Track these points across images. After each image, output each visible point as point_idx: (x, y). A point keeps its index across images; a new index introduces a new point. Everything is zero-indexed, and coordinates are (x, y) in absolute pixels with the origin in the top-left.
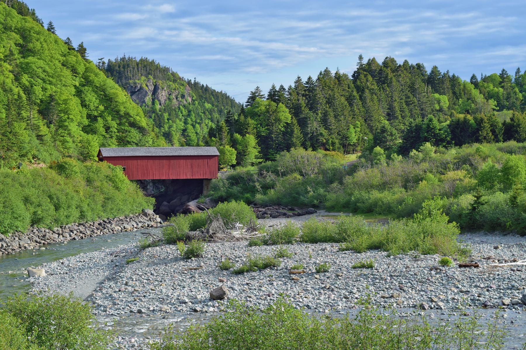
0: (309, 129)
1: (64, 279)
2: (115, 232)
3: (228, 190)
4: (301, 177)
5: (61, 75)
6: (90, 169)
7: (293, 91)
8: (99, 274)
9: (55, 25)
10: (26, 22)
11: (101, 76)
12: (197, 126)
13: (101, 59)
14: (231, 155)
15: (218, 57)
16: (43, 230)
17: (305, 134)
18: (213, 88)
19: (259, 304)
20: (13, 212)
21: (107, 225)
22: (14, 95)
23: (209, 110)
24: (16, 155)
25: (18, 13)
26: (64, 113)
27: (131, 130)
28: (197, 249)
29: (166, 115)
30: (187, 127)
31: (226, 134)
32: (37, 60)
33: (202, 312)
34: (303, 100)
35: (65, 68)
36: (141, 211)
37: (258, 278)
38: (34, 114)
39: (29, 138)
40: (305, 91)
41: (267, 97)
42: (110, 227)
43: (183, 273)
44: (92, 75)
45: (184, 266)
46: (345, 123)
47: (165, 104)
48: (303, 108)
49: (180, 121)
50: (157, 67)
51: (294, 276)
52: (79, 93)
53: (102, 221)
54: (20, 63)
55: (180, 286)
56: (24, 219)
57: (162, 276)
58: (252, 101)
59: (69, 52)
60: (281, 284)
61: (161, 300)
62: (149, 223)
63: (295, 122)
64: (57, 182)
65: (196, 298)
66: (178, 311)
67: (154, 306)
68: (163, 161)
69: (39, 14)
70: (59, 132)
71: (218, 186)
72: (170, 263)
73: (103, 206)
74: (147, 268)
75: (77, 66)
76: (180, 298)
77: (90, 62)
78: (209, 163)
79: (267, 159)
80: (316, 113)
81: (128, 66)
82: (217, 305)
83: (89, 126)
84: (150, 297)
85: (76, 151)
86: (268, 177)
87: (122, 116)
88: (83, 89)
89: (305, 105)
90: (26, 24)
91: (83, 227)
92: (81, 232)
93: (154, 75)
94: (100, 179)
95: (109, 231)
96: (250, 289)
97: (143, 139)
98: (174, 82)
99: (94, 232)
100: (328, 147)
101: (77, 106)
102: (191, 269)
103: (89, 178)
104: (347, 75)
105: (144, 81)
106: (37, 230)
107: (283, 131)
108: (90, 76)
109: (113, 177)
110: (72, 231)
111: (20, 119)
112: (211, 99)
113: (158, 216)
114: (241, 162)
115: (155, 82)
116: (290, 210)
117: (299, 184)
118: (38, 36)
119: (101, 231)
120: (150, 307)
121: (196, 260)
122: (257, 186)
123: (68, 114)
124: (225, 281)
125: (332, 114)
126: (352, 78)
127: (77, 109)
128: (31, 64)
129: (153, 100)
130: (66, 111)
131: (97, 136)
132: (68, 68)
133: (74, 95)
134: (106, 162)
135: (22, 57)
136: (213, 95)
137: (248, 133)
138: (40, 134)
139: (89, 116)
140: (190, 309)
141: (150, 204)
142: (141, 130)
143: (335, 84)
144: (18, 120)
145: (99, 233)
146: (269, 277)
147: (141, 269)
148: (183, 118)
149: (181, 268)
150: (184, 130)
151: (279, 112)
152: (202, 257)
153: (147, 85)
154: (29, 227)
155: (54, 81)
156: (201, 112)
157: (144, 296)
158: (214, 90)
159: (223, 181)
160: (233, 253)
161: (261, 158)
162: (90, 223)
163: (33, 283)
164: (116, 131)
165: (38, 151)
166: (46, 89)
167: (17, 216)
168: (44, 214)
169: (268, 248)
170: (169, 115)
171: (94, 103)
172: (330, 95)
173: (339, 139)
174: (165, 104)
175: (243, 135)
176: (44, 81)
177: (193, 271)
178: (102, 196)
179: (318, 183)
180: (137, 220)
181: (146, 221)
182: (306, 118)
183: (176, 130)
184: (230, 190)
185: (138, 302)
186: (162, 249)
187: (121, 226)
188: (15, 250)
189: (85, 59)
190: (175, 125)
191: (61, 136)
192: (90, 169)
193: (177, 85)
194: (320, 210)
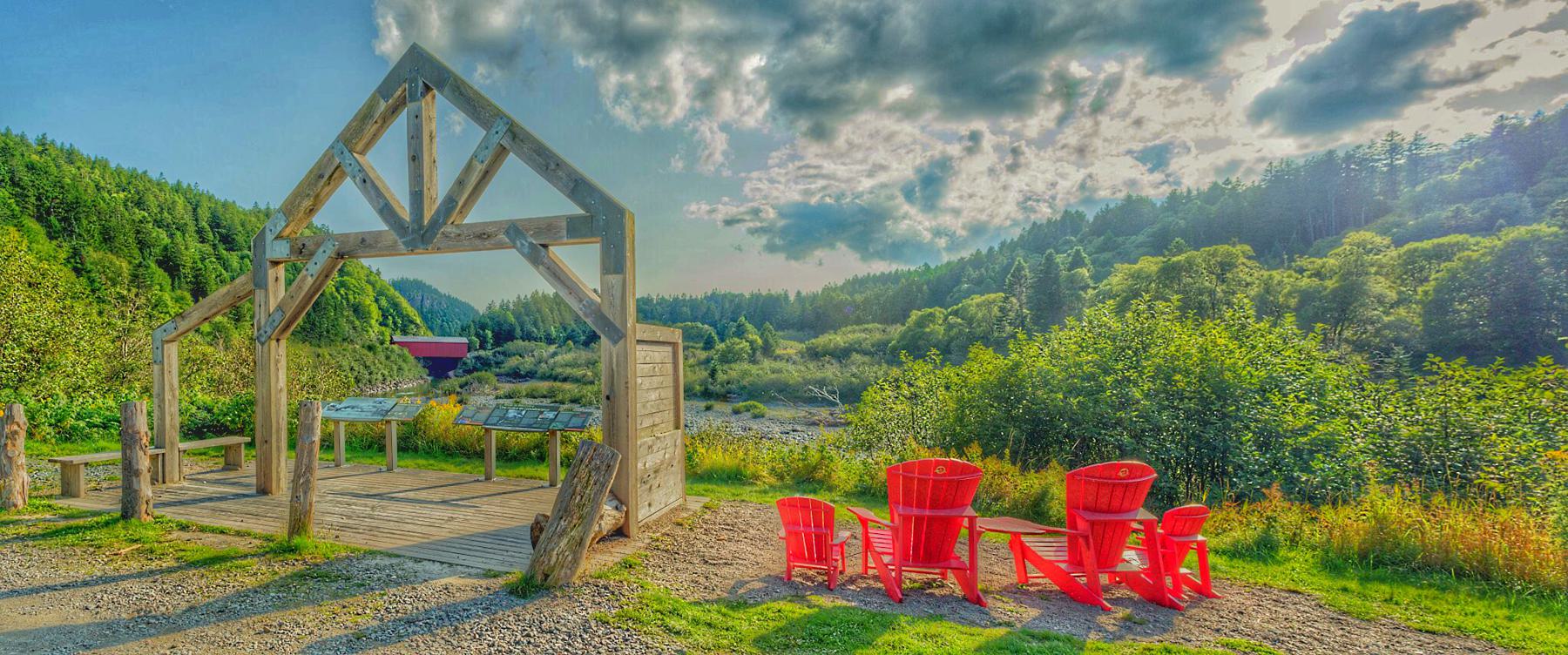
52: (377, 301)
142: (417, 325)
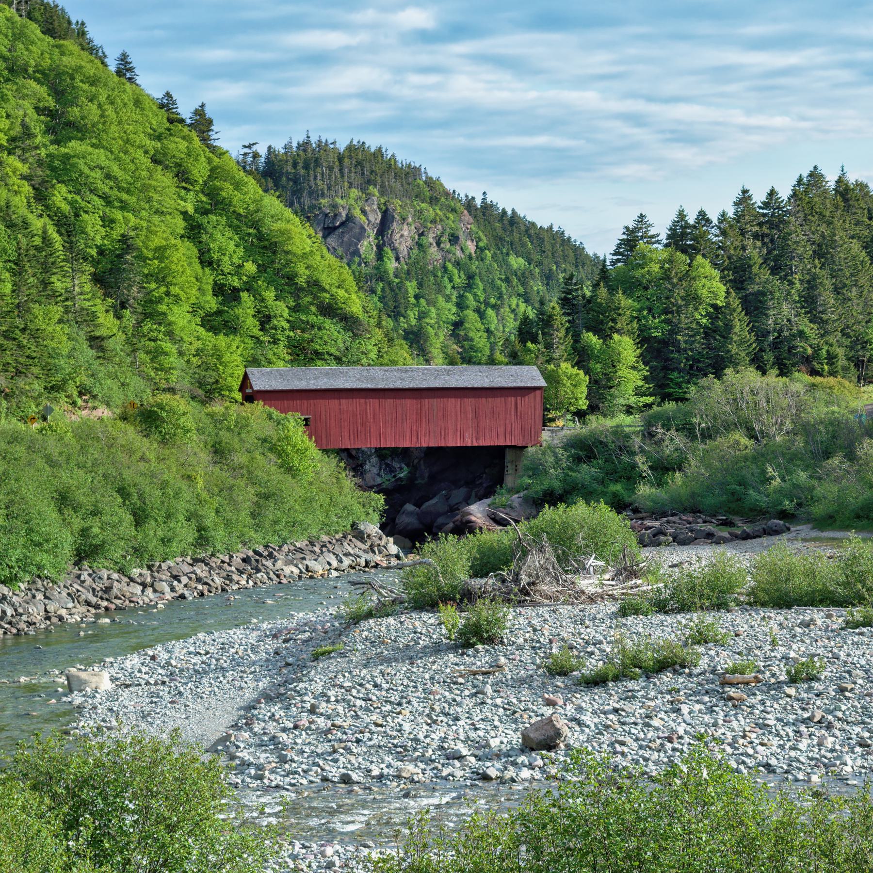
0: (771, 322)
1: (158, 697)
2: (284, 581)
6: (221, 422)
7: (731, 226)
8: (243, 684)
9: (135, 60)
10: (63, 54)
11: (250, 187)
12: (490, 312)
14: (575, 386)
15: (541, 140)
16: (105, 573)
19: (646, 760)
20: (30, 530)
21: (264, 562)
23: (519, 274)
24: (36, 387)
25: (43, 32)
26: (157, 281)
27: (324, 322)
28: (489, 623)
29: (411, 287)
31: (562, 333)
32: (90, 149)
33: (502, 781)
34: (755, 248)
35: (160, 168)
36: (349, 527)
37: (643, 696)
38: (83, 283)
39: (70, 345)
40: (760, 224)
41: (665, 241)
43: (455, 683)
45: (457, 664)
46: (861, 305)
47: (410, 258)
48: (755, 269)
49: (447, 301)
50: (390, 166)
51: (733, 690)
53: (251, 553)
54: (48, 156)
55: (447, 715)
56: (56, 546)
57: (402, 691)
58: (627, 251)
59: (169, 130)
60: (700, 711)
61: (399, 749)
62: (369, 556)
63: (736, 303)
64: (138, 455)
65: (488, 745)
67: (383, 766)
69: (96, 34)
70: (145, 329)
71: (541, 464)
72: (421, 658)
73: (253, 515)
74: (365, 671)
75: (189, 164)
76: (446, 745)
77: (221, 154)
79: (666, 397)
82: (540, 762)
83: (219, 313)
84: (371, 743)
85: (188, 378)
86: (667, 442)
87: (301, 289)
88: (204, 220)
89: (760, 261)
90: (64, 59)
92: (199, 580)
94: (247, 446)
95: (269, 578)
96: (624, 724)
97: (355, 345)
98: (431, 203)
99: (231, 581)
101: (190, 264)
102: (475, 674)
103: (220, 443)
105: (356, 201)
106: (90, 575)
107: (706, 327)
108: (222, 189)
109: (279, 440)
110: (176, 578)
111: (48, 297)
112: (524, 245)
113: (391, 540)
114: (601, 405)
115: (385, 204)
116: (722, 524)
118: (93, 89)
119: (250, 576)
120: (373, 767)
121: (487, 651)
122: (641, 465)
124: (561, 702)
125: (828, 283)
128: (76, 160)
129: (380, 248)
130: (161, 278)
131: (238, 339)
132: (167, 167)
133: (182, 236)
134: (261, 403)
136: (530, 237)
137: (618, 331)
138: (98, 334)
139: (219, 289)
141: (371, 511)
142: (349, 322)
144: (43, 300)
145: (243, 582)
146: (669, 692)
147: (350, 672)
148: (455, 293)
149: (448, 670)
150: (458, 325)
151: (694, 278)
152: (502, 643)
153: (363, 212)
154: (70, 567)
155: (132, 200)
156: (500, 279)
157: (358, 741)
158: (533, 224)
159: (554, 452)
161: (651, 395)
164: (286, 325)
165: (92, 375)
166: (112, 221)
168: (109, 535)
169: (669, 619)
170: (420, 285)
171: (231, 257)
172: (823, 236)
173: (846, 347)
174: (410, 258)
175: (605, 336)
176: (107, 200)
177: (481, 678)
178: (251, 490)
179: (793, 458)
180: (338, 550)
181: (361, 553)
182: (763, 294)
184: (573, 474)
185: (342, 754)
186: (401, 623)
188: (35, 623)
191: (150, 340)
192: (221, 422)
193: (438, 211)
194: (798, 524)
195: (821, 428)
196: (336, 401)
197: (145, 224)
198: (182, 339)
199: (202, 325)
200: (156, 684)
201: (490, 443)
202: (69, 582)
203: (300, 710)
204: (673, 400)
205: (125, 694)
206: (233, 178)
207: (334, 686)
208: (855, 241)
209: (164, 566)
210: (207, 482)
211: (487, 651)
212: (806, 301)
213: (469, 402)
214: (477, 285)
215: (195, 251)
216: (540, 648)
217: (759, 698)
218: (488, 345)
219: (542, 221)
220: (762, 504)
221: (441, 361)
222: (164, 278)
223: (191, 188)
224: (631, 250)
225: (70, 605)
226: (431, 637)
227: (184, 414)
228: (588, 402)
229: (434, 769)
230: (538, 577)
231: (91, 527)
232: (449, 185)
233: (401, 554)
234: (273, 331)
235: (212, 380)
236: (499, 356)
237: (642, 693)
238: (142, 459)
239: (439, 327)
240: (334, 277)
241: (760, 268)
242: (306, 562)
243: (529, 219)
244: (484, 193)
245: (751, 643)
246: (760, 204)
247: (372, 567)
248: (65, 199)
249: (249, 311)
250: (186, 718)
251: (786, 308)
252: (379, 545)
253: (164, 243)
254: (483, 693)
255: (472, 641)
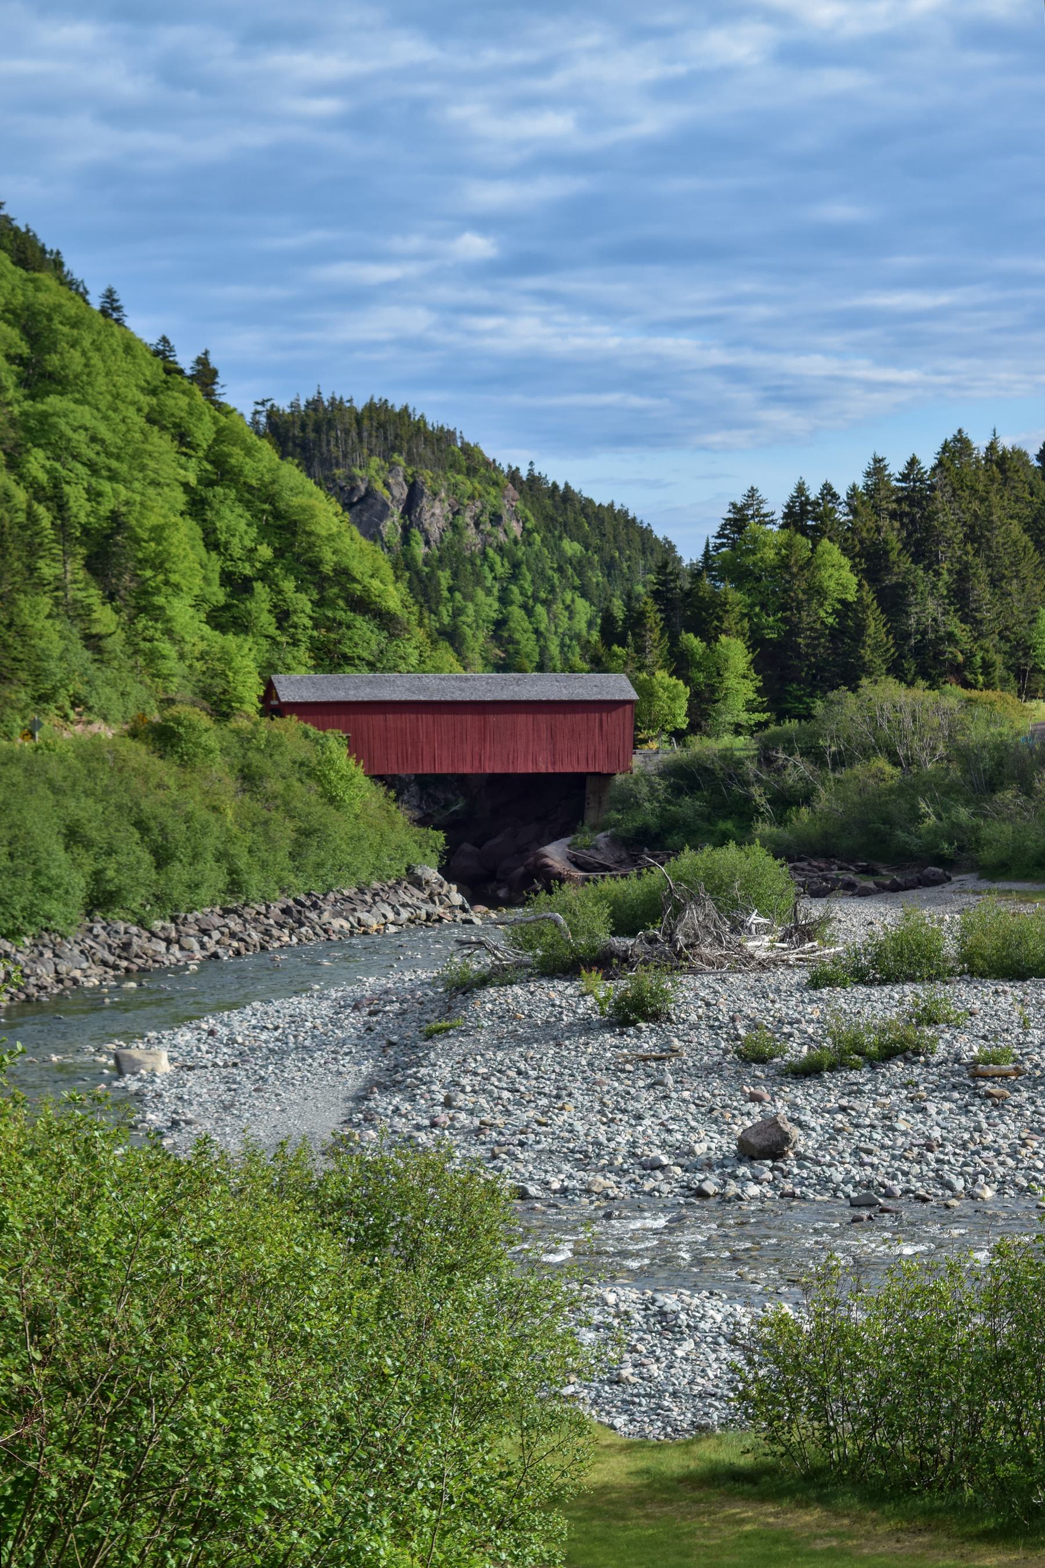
0: (912, 621)
1: (235, 1082)
2: (334, 937)
3: (664, 809)
4: (896, 771)
5: (145, 451)
6: (249, 741)
7: (863, 503)
8: (342, 1069)
9: (123, 298)
10: (38, 289)
11: (265, 453)
12: (540, 609)
13: (263, 404)
14: (673, 700)
15: (612, 398)
16: (121, 926)
17: (901, 636)
18: (586, 494)
19: (905, 1174)
20: (37, 873)
21: (308, 914)
22: (16, 512)
23: (574, 562)
24: (22, 696)
25: (14, 263)
26: (154, 567)
27: (354, 620)
28: (654, 995)
29: (444, 577)
30: (509, 613)
31: (656, 635)
32: (72, 406)
33: (724, 1199)
34: (893, 529)
35: (156, 428)
36: (404, 871)
37: (871, 1091)
38: (75, 569)
39: (62, 644)
40: (898, 501)
41: (781, 522)
42: (317, 920)
43: (623, 1071)
44: (236, 450)
45: (617, 1047)
46: (1024, 600)
47: (442, 541)
48: (893, 556)
49: (487, 595)
50: (419, 428)
51: (989, 1084)
53: (291, 903)
54: (22, 414)
55: (624, 1111)
56: (67, 892)
57: (556, 1080)
58: (734, 533)
59: (166, 382)
60: (951, 1111)
61: (578, 1156)
62: (430, 907)
63: (869, 597)
64: (153, 781)
65: (691, 1152)
66: (645, 1193)
67: (562, 1176)
68: (464, 717)
69: (75, 265)
70: (140, 626)
71: (631, 796)
72: (568, 1038)
73: (292, 856)
74: (500, 1055)
75: (191, 424)
76: (639, 1151)
77: (228, 412)
78: (605, 724)
79: (781, 716)
80: (934, 571)
81: (331, 424)
82: (769, 1175)
83: (227, 607)
84: (540, 1147)
85: (190, 686)
86: (790, 770)
87: (325, 578)
88: (209, 493)
89: (900, 546)
90: (40, 295)
91: (239, 921)
92: (233, 935)
93: (409, 453)
94: (282, 770)
95: (316, 934)
96: (857, 1126)
97: (392, 648)
98: (468, 475)
99: (271, 936)
100: (970, 677)
101: (193, 547)
102: (645, 1059)
103: (249, 766)
104: (1025, 454)
105: (377, 471)
106: (104, 928)
107: (832, 627)
108: (230, 455)
109: (319, 763)
110: (205, 932)
111: (35, 585)
112: (580, 527)
113: (454, 887)
114: (703, 723)
115: (412, 476)
116: (862, 872)
117: (891, 790)
118: (75, 332)
119: (292, 932)
120: (549, 1178)
121: (652, 1030)
122: (757, 798)
123: (167, 571)
124: (768, 1098)
125: (983, 573)
126: (1037, 464)
127: (192, 557)
128: (55, 419)
129: (406, 529)
130: (159, 564)
131: (250, 639)
132: (163, 428)
133: (182, 514)
134: (295, 717)
135: (26, 397)
136: (586, 516)
137: (726, 632)
138: (94, 631)
139: (227, 578)
140: (682, 1187)
141: (428, 851)
142: (385, 620)
143: (992, 480)
144: (29, 589)
145: (286, 939)
146: (905, 1086)
147: (482, 1055)
148: (497, 585)
149: (609, 1055)
150: (500, 624)
151: (818, 567)
152: (671, 1021)
153: (387, 485)
154: (80, 920)
155: (122, 468)
156: (552, 568)
157: (522, 1144)
158: (590, 501)
159: (648, 781)
160: (768, 1010)
161: (764, 711)
162: (256, 906)
163: (139, 1095)
164: (309, 623)
165: (88, 682)
166: (100, 494)
167: (50, 885)
168: (124, 879)
169: (875, 992)
170: (455, 575)
171: (241, 539)
172: (975, 515)
173: (1005, 653)
174: (442, 541)
175: (710, 637)
176: (93, 468)
177: (654, 1064)
178: (290, 825)
179: (951, 790)
180: (393, 899)
181: (420, 904)
182: (904, 587)
183: (476, 621)
184: (672, 808)
185: (505, 1161)
186: (532, 993)
187: (351, 919)
188: (46, 988)
189: (214, 403)
190: (471, 608)
191: (144, 639)
192: (249, 741)
193: (477, 485)
194: (959, 873)
195: (985, 754)
196: (381, 717)
197: (138, 498)
198: (183, 640)
199: (207, 623)
200: (226, 1066)
201: (570, 770)
202: (80, 937)
203: (430, 1103)
204: (795, 717)
205: (191, 1077)
206: (244, 441)
207: (466, 1072)
208: (1015, 522)
209: (191, 918)
210: (236, 815)
211: (652, 1030)
212: (955, 596)
213: (543, 719)
214: (524, 575)
215: (198, 532)
216: (720, 1028)
217: (1026, 1095)
218: (538, 650)
219: (600, 497)
220: (912, 847)
221: (480, 668)
222: (162, 563)
223: (192, 453)
224: (740, 532)
225: (85, 965)
226: (574, 1012)
227: (206, 730)
228: (688, 720)
229: (630, 1181)
230: (697, 936)
231: (105, 869)
232: (490, 453)
233: (467, 906)
234: (292, 630)
235: (218, 690)
236: (576, 660)
237: (869, 1087)
238: (160, 786)
239: (478, 627)
240: (367, 564)
241: (899, 555)
242: (358, 914)
243: (585, 494)
244: (531, 463)
245: (995, 1024)
246: (898, 476)
247: (435, 921)
248: (43, 467)
249: (263, 605)
250: (283, 1111)
251: (931, 604)
252: (439, 894)
253: (162, 521)
254: (661, 1083)
255: (633, 1016)
